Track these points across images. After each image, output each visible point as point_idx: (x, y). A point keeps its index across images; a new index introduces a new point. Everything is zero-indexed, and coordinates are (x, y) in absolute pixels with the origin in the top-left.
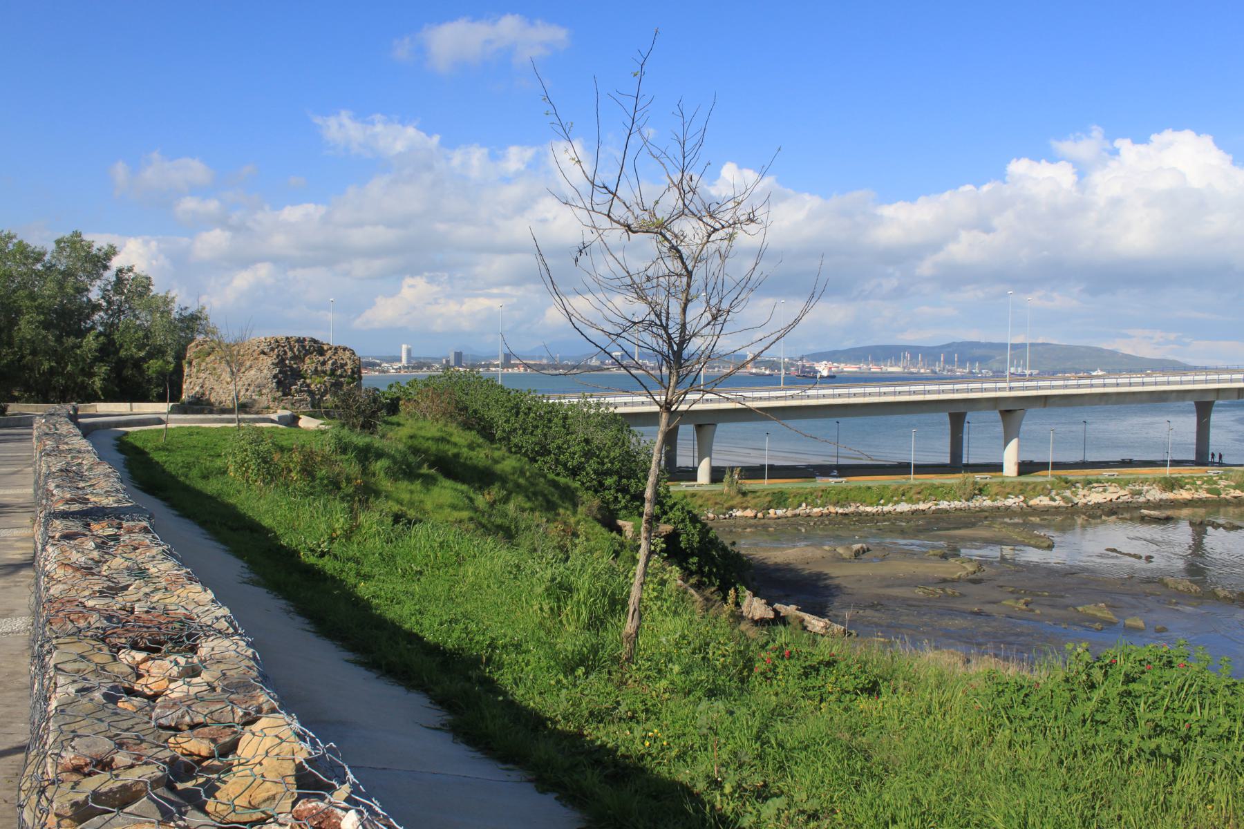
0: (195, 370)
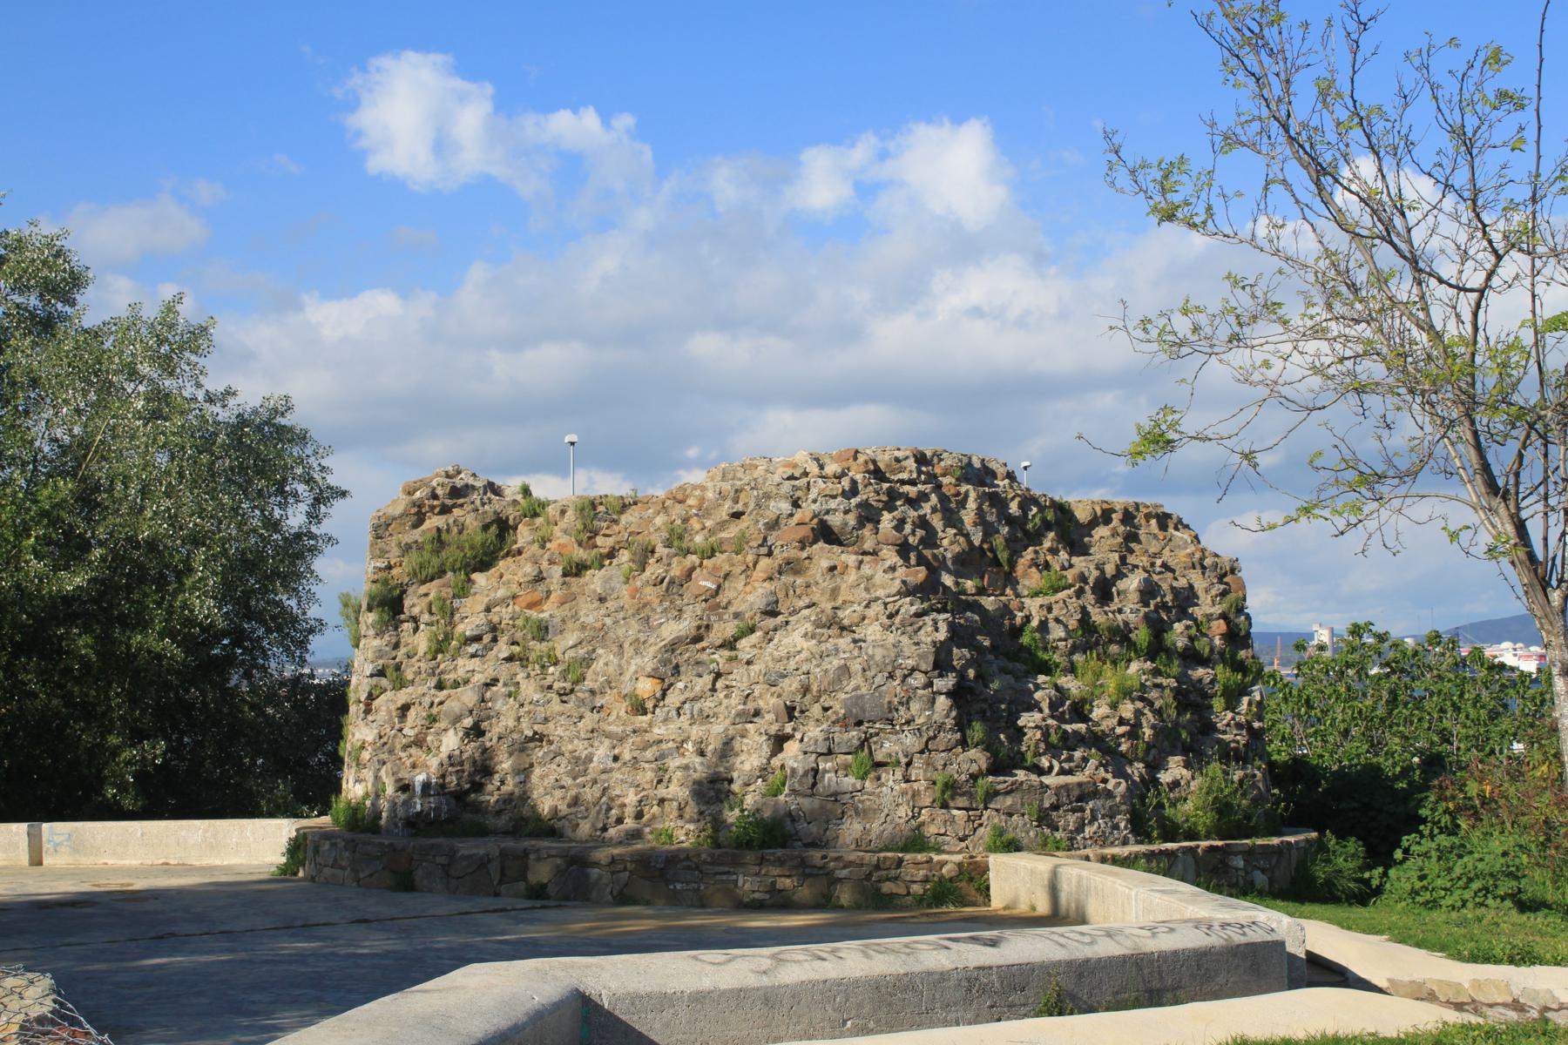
0: (422, 642)
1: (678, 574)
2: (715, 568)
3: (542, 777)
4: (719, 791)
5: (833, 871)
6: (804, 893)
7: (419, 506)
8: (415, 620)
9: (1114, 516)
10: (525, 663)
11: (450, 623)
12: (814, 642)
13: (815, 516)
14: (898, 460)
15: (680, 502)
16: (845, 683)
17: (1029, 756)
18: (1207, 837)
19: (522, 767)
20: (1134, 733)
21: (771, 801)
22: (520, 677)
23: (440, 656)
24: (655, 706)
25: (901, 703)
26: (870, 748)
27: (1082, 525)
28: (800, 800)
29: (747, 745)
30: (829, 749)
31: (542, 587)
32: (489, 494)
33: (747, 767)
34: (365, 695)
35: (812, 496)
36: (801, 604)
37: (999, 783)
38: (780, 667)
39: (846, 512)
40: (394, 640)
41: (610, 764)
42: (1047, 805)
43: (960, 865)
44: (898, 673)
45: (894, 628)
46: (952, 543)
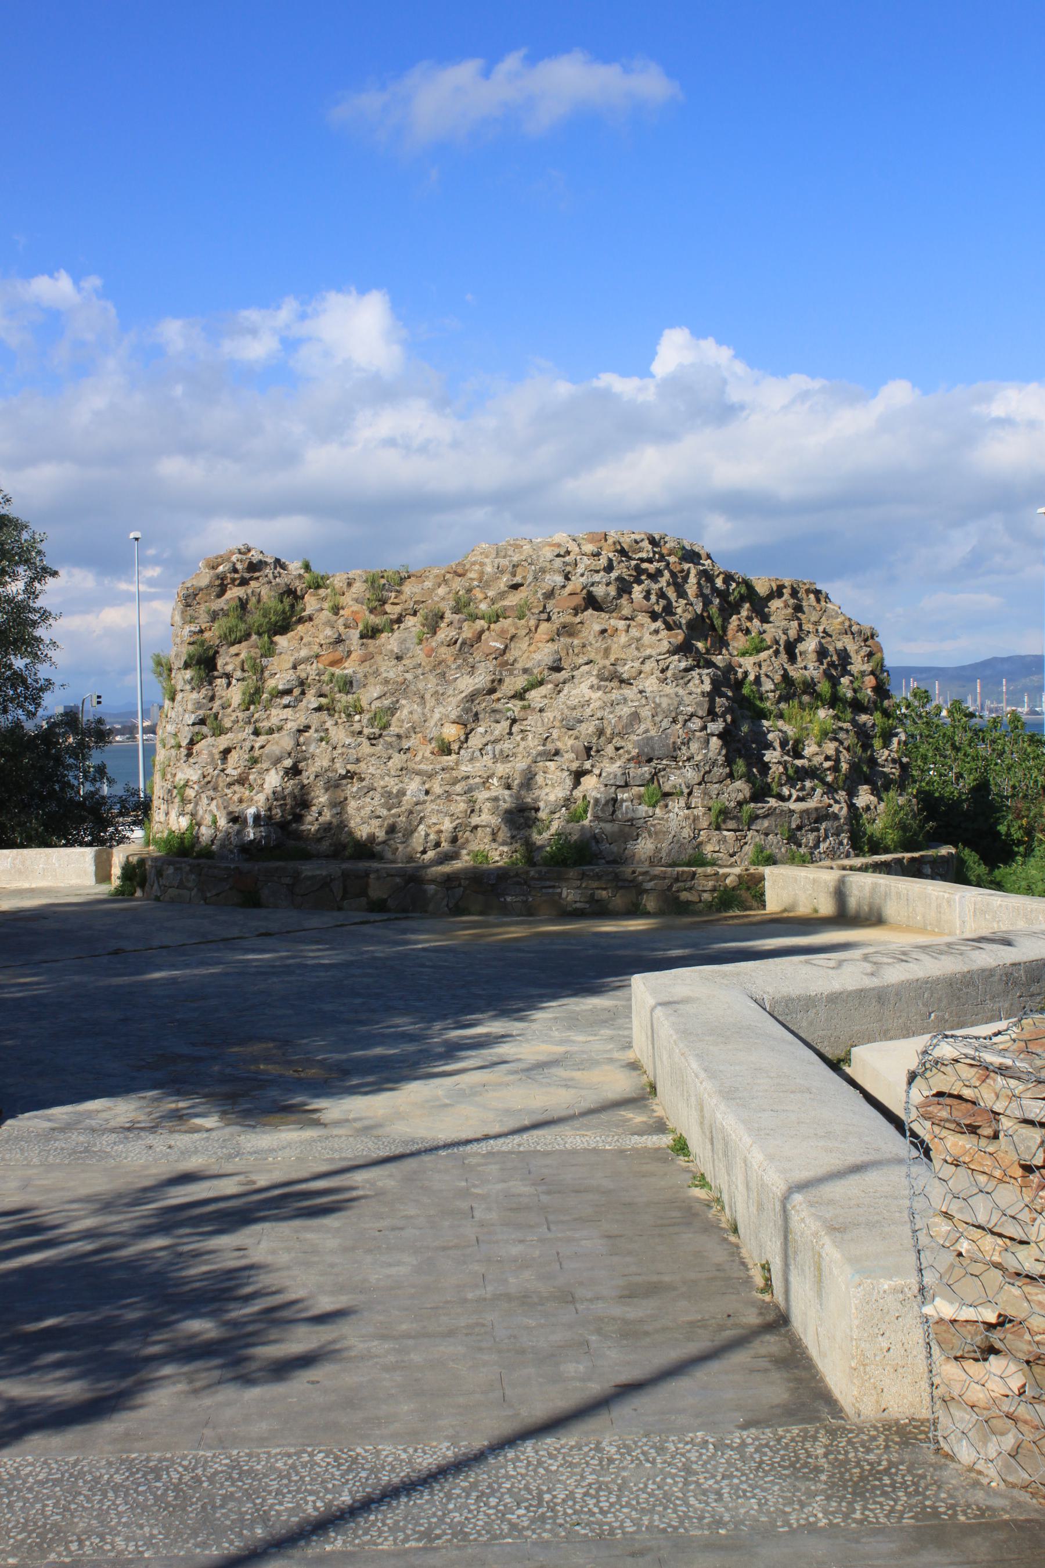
0: (235, 695)
1: (470, 635)
2: (503, 631)
3: (359, 809)
4: (528, 819)
5: (641, 883)
6: (619, 901)
7: (222, 579)
8: (228, 676)
9: (785, 591)
10: (332, 712)
11: (261, 678)
12: (601, 693)
13: (584, 588)
14: (636, 542)
15: (460, 576)
16: (636, 727)
17: (774, 785)
18: (895, 851)
19: (338, 800)
20: (836, 769)
21: (576, 826)
22: (329, 724)
23: (252, 707)
24: (460, 748)
25: (683, 743)
26: (658, 781)
27: (761, 598)
28: (602, 825)
29: (552, 779)
30: (626, 782)
31: (341, 648)
32: (278, 569)
33: (552, 798)
34: (187, 741)
35: (580, 571)
36: (581, 661)
37: (759, 809)
38: (577, 714)
39: (608, 584)
40: (210, 694)
41: (422, 797)
42: (794, 826)
43: (740, 876)
44: (681, 718)
45: (669, 681)
46: (684, 611)
